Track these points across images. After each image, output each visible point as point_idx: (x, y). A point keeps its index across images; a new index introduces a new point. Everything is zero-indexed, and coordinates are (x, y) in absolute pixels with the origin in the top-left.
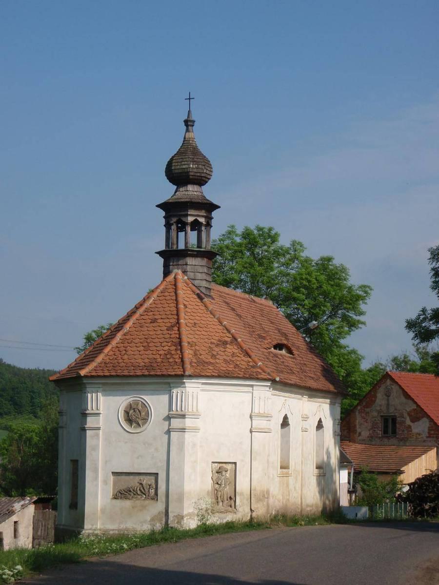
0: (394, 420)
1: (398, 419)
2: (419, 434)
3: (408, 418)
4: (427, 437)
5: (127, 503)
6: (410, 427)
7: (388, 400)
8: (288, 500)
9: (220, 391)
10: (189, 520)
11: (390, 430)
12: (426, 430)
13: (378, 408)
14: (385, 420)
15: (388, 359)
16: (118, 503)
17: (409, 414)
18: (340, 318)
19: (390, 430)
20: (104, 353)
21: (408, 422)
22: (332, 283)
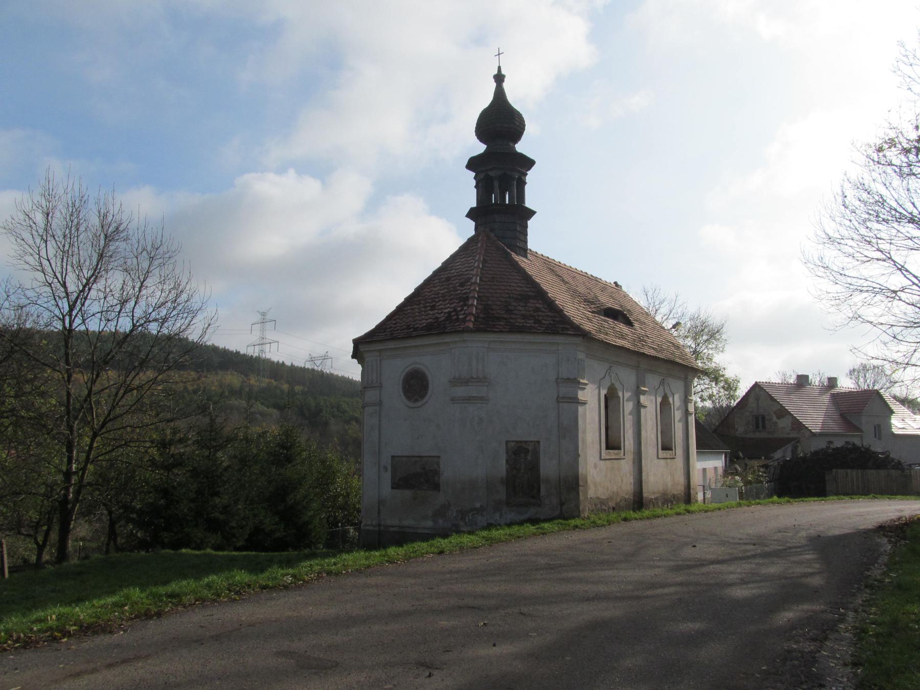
0: (763, 418)
1: (767, 417)
2: (784, 428)
3: (774, 416)
4: (791, 430)
5: (408, 493)
6: (776, 423)
7: (758, 403)
8: (620, 487)
9: (624, 430)
10: (476, 516)
11: (760, 425)
12: (790, 425)
13: (750, 410)
14: (757, 418)
15: (792, 374)
16: (398, 492)
17: (775, 413)
18: (25, 520)
19: (760, 425)
20: (678, 409)
21: (775, 419)
22: (705, 337)
